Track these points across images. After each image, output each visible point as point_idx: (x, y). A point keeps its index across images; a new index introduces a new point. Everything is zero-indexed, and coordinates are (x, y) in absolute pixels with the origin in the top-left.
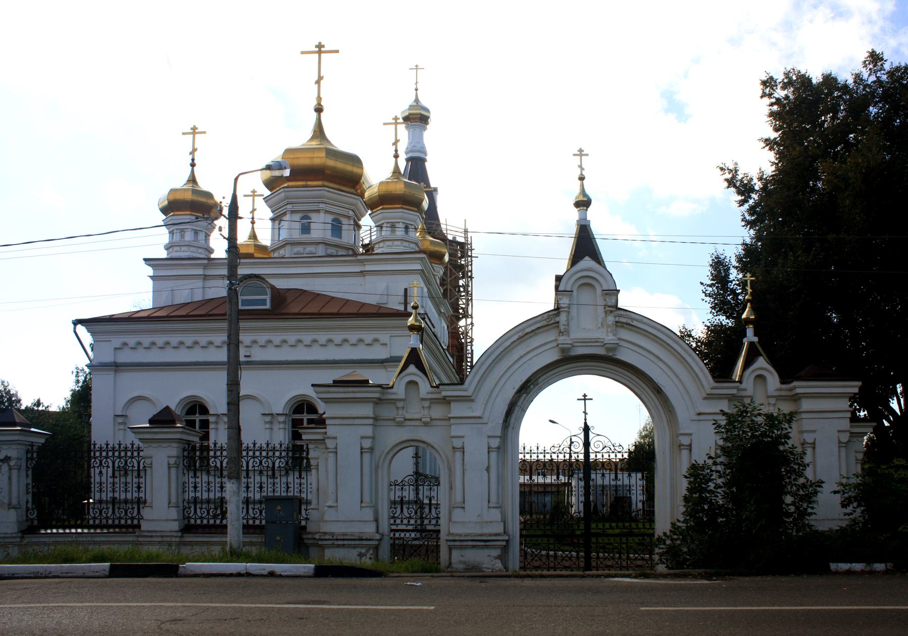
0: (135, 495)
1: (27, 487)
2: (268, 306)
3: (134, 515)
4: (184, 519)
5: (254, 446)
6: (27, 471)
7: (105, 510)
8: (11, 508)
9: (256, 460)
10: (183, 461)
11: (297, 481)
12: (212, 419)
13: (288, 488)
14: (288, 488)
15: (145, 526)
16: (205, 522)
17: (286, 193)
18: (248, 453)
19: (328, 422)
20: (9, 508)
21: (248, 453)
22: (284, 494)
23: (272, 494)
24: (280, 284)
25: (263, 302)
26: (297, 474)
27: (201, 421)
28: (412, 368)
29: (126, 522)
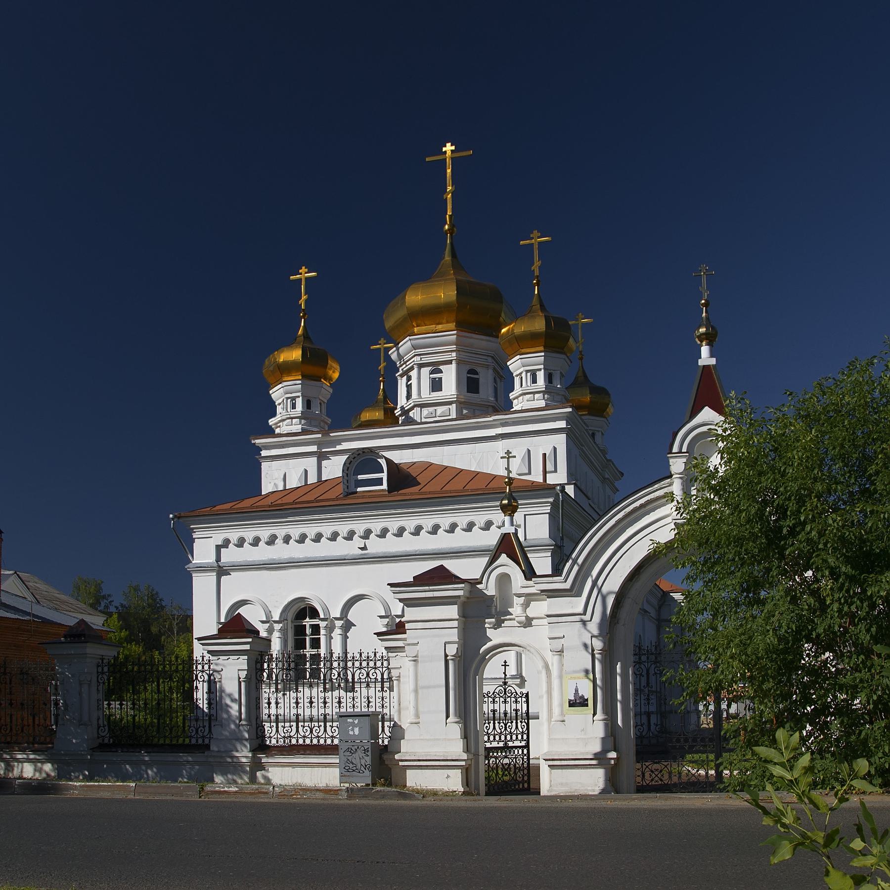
0: (322, 711)
1: (98, 703)
2: (385, 486)
3: (205, 734)
4: (257, 738)
5: (361, 655)
6: (98, 686)
7: (201, 728)
8: (82, 725)
9: (363, 671)
10: (256, 673)
11: (379, 694)
12: (323, 624)
13: (369, 702)
14: (369, 702)
15: (214, 748)
16: (308, 741)
17: (413, 342)
18: (353, 664)
19: (407, 626)
20: (80, 725)
21: (353, 664)
22: (365, 710)
23: (352, 710)
24: (398, 457)
25: (379, 482)
26: (321, 688)
27: (312, 626)
28: (504, 558)
29: (297, 741)
